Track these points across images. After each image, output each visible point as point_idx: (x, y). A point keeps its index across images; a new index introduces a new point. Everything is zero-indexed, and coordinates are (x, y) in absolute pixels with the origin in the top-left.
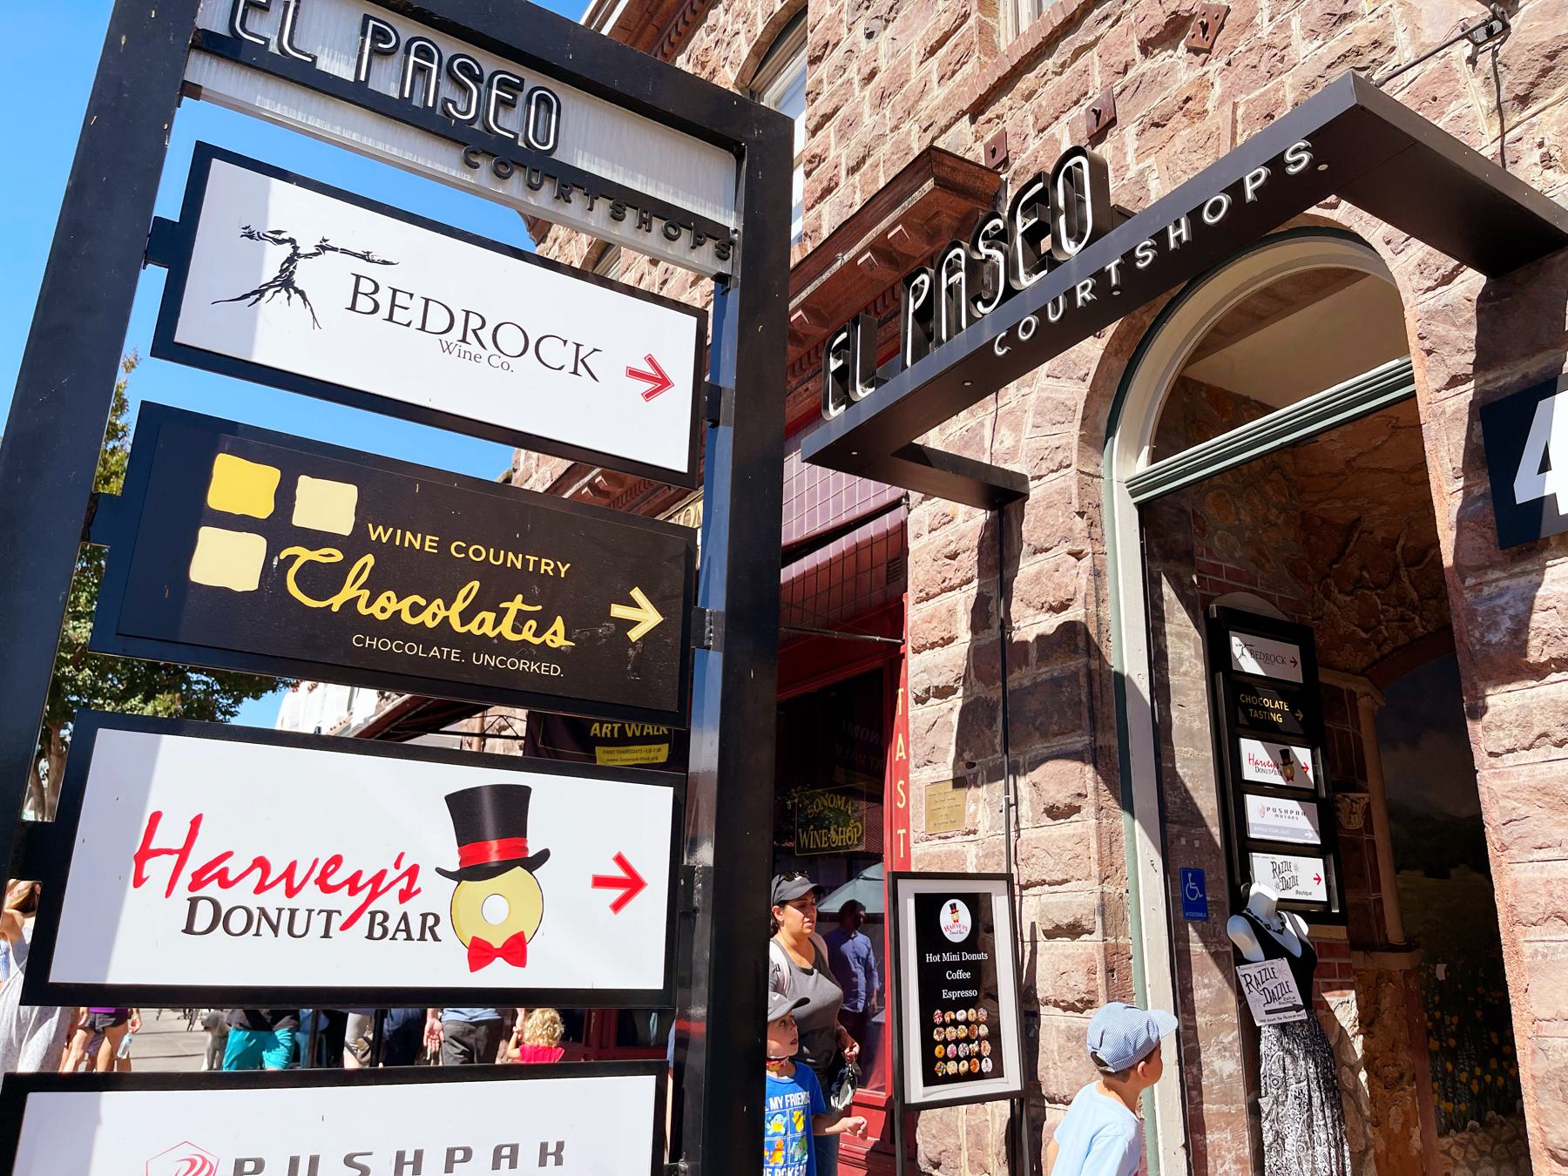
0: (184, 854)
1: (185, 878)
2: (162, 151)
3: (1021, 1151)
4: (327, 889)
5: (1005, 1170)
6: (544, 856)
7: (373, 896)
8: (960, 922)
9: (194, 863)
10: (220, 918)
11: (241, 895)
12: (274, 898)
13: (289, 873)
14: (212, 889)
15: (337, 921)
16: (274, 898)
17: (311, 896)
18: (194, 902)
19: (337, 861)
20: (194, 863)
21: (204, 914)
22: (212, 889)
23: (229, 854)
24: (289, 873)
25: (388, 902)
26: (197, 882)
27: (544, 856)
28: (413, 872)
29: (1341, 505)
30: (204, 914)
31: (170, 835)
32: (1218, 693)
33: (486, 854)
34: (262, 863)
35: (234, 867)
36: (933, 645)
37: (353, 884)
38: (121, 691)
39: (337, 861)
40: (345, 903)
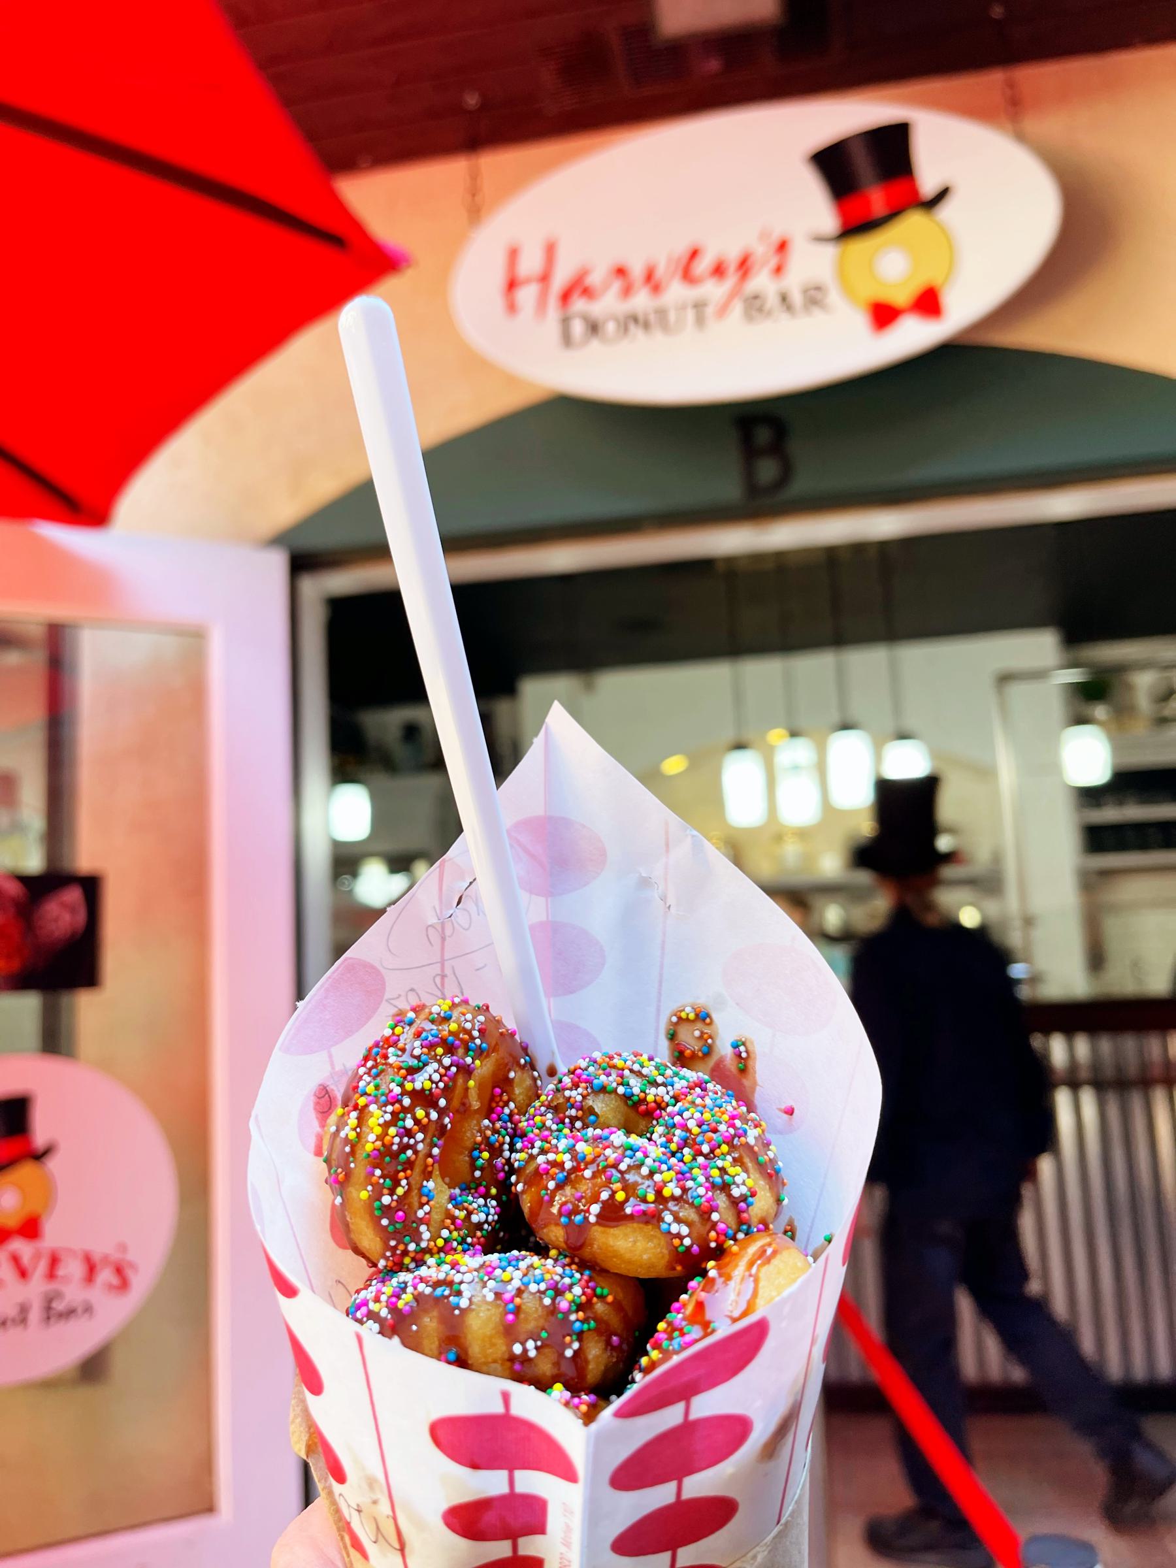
0: (545, 278)
2: (403, 358)
5: (1174, 670)
6: (943, 194)
8: (53, 1234)
10: (594, 328)
11: (608, 304)
13: (649, 276)
14: (579, 305)
15: (710, 311)
16: (642, 301)
17: (676, 292)
18: (566, 322)
19: (694, 254)
20: (561, 278)
21: (578, 327)
24: (649, 276)
25: (762, 281)
27: (943, 194)
28: (782, 247)
30: (578, 327)
31: (530, 263)
33: (867, 203)
34: (621, 272)
35: (595, 279)
36: (481, 949)
37: (719, 271)
39: (694, 254)
40: (714, 291)
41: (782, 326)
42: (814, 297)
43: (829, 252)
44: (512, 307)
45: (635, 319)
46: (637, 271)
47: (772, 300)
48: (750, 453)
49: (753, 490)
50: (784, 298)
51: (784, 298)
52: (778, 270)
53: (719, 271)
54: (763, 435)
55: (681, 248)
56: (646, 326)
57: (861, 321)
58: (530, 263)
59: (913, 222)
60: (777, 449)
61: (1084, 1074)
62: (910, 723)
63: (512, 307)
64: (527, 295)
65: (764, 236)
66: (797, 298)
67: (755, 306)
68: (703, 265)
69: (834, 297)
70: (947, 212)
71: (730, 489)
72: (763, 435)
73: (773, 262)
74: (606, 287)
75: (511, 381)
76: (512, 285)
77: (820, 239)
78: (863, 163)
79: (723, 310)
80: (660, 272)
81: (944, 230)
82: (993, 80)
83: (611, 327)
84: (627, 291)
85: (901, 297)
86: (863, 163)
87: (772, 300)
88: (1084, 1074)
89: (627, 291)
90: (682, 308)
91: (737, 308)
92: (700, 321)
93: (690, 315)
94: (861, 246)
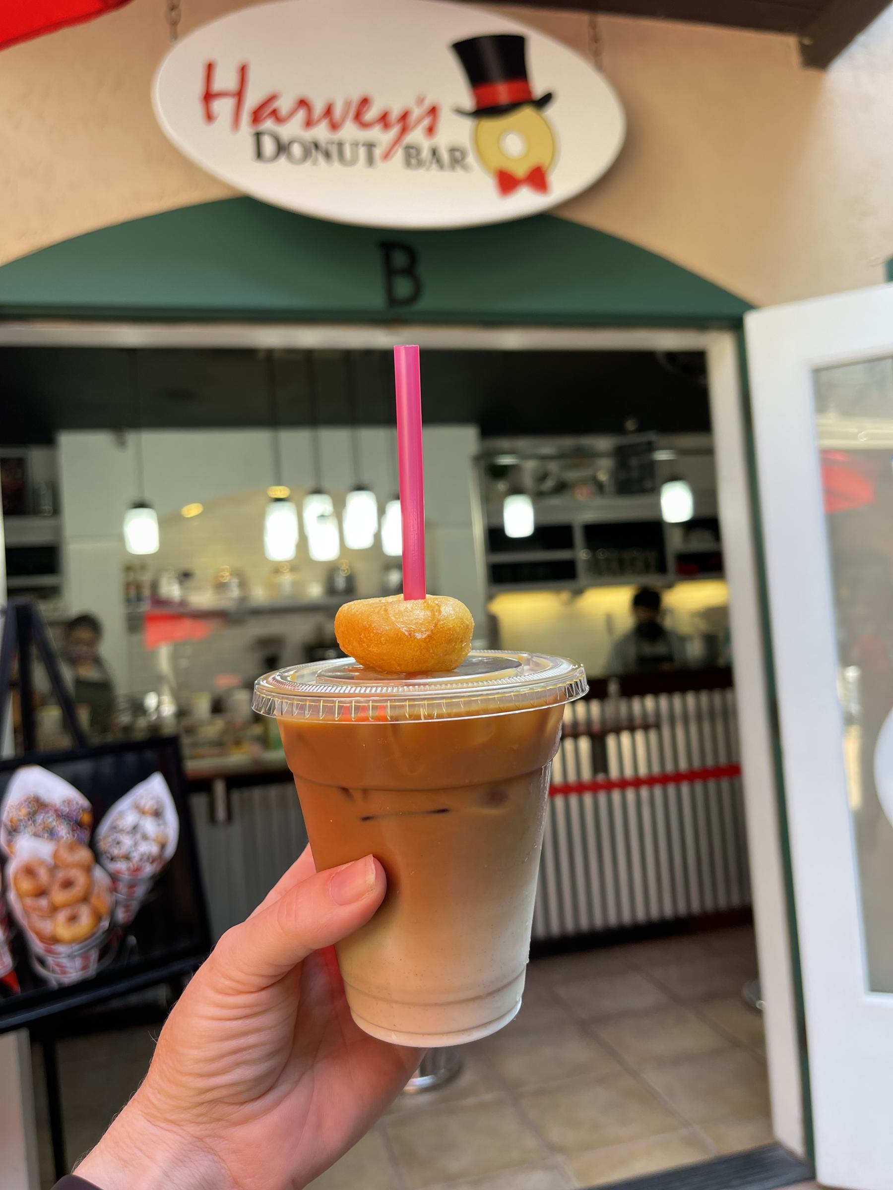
0: (240, 95)
1: (246, 117)
3: (337, 684)
4: (365, 125)
7: (404, 131)
9: (252, 100)
10: (282, 148)
11: (292, 129)
12: (321, 132)
13: (328, 112)
14: (268, 124)
15: (378, 152)
16: (321, 132)
17: (350, 131)
18: (258, 136)
19: (365, 102)
20: (252, 100)
21: (269, 146)
22: (268, 124)
23: (272, 98)
24: (328, 112)
25: (416, 136)
26: (256, 116)
27: (546, 100)
28: (433, 111)
29: (417, 634)
30: (269, 146)
31: (225, 80)
32: (339, 675)
34: (303, 103)
35: (284, 105)
37: (384, 120)
38: (159, 694)
39: (365, 102)
40: (382, 137)
41: (431, 175)
42: (457, 158)
43: (468, 124)
44: (209, 117)
45: (316, 146)
46: (318, 108)
47: (425, 154)
48: (390, 272)
49: (392, 301)
50: (434, 152)
51: (434, 152)
52: (431, 130)
53: (384, 120)
54: (400, 259)
55: (356, 97)
56: (327, 155)
57: (490, 184)
58: (225, 80)
59: (527, 114)
60: (410, 271)
61: (582, 728)
62: (366, 478)
63: (209, 117)
64: (223, 107)
65: (420, 101)
66: (445, 156)
67: (412, 156)
68: (371, 114)
69: (471, 159)
70: (552, 111)
71: (376, 299)
72: (400, 259)
73: (426, 122)
74: (292, 114)
75: (213, 180)
76: (208, 97)
77: (460, 112)
78: (492, 61)
79: (387, 156)
80: (338, 112)
81: (548, 126)
82: (577, 20)
83: (296, 150)
84: (309, 123)
85: (520, 170)
86: (492, 61)
87: (425, 154)
88: (582, 728)
89: (309, 123)
90: (355, 145)
91: (399, 155)
92: (370, 160)
93: (362, 152)
94: (491, 125)
